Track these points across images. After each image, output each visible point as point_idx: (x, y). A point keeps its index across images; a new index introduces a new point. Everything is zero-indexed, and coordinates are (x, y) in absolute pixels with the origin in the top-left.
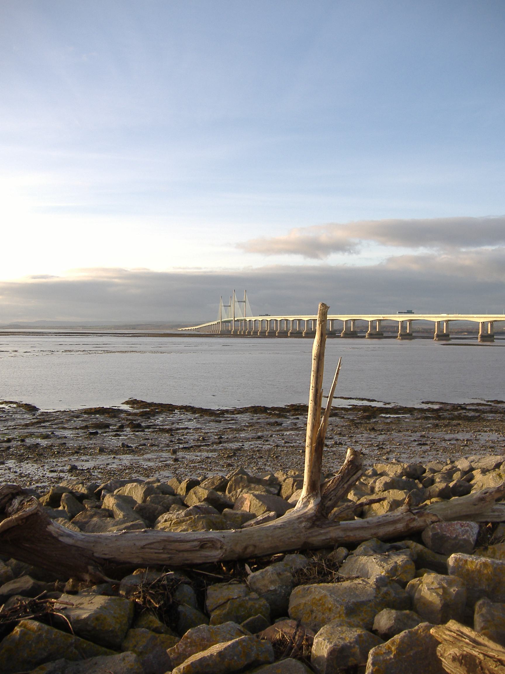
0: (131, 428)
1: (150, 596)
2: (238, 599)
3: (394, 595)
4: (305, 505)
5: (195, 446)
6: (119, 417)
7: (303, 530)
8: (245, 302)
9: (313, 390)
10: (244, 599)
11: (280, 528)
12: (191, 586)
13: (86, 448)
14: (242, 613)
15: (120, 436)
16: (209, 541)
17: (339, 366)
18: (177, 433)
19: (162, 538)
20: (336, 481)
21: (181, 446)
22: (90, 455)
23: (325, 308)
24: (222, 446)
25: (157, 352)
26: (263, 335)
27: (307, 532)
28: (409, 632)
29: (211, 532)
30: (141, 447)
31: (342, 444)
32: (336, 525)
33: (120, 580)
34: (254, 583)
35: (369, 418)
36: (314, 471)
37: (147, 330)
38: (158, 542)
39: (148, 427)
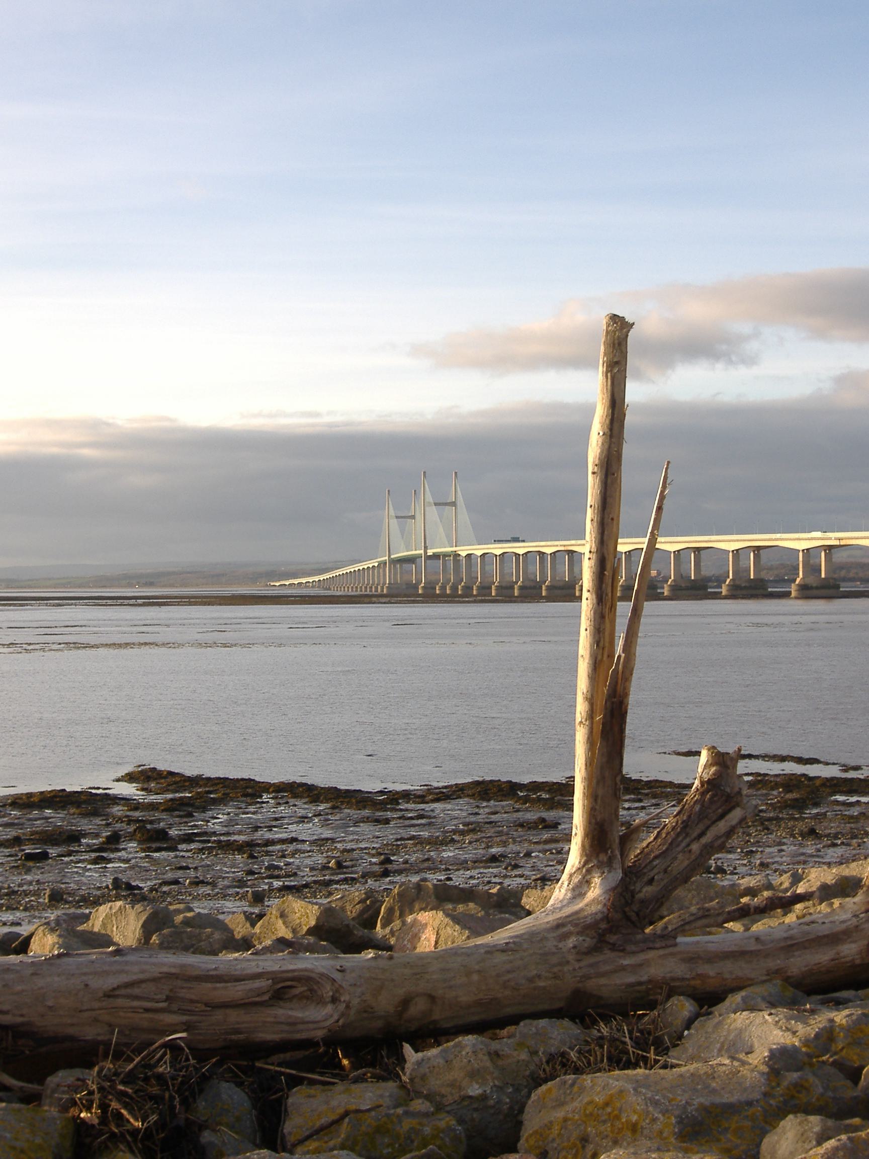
0: (140, 842)
1: (119, 1101)
2: (373, 1113)
3: (821, 1090)
4: (578, 891)
5: (315, 882)
6: (107, 816)
7: (571, 958)
8: (453, 504)
9: (593, 562)
10: (392, 1111)
11: (503, 951)
12: (243, 1090)
13: (14, 892)
14: (385, 1151)
15: (110, 861)
16: (298, 979)
17: (664, 487)
18: (268, 853)
19: (165, 969)
20: (668, 833)
21: (277, 884)
22: (26, 909)
23: (622, 328)
24: (391, 882)
25: (215, 644)
26: (506, 595)
27: (583, 964)
28: (849, 1138)
29: (307, 958)
30: (165, 889)
31: (723, 872)
32: (667, 947)
33: (41, 1081)
34: (423, 1077)
35: (799, 805)
36: (600, 792)
37: (186, 587)
38: (154, 980)
39: (188, 839)
